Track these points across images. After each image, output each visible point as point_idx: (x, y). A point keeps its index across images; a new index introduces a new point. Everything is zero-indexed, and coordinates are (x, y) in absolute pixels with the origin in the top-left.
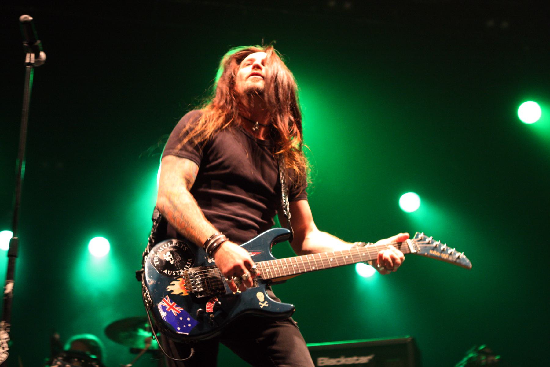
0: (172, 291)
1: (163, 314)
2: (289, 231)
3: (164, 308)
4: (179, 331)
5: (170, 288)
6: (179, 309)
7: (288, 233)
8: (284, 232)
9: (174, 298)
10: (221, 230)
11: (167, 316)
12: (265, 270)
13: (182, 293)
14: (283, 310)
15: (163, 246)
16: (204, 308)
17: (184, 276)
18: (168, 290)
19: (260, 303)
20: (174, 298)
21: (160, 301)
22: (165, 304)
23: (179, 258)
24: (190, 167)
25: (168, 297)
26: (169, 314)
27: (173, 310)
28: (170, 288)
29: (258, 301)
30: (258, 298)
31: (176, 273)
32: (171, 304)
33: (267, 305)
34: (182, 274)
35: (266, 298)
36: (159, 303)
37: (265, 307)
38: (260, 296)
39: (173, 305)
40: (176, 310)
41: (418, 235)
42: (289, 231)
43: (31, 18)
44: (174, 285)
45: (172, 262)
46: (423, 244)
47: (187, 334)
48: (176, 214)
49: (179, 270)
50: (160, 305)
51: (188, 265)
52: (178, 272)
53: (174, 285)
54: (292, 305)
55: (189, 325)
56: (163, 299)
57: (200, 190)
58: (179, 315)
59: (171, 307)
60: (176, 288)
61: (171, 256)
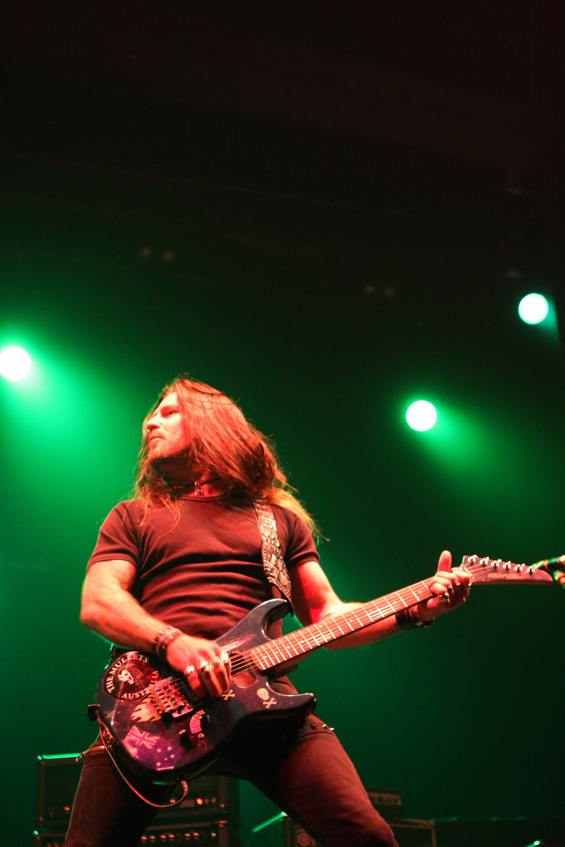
0: (139, 718)
1: (133, 751)
2: (286, 601)
3: (132, 743)
4: (160, 767)
5: (136, 715)
6: (155, 739)
7: (284, 603)
8: (278, 604)
9: (142, 726)
10: (169, 622)
11: (139, 753)
12: (261, 657)
13: (153, 718)
14: (299, 703)
15: (116, 665)
16: (188, 728)
17: (150, 694)
18: (134, 718)
19: (265, 703)
20: (142, 726)
21: (125, 734)
22: (133, 738)
23: (140, 674)
24: (122, 567)
25: (135, 728)
26: (142, 748)
27: (139, 735)
28: (136, 715)
29: (261, 700)
30: (261, 697)
31: (140, 694)
32: (141, 736)
33: (275, 703)
34: (148, 692)
35: (271, 694)
36: (124, 737)
37: (272, 705)
38: (263, 693)
39: (145, 736)
40: (150, 741)
41: (466, 560)
42: (286, 601)
43: (184, 731)
44: (140, 710)
45: (131, 682)
46: (474, 568)
47: (172, 768)
48: (111, 617)
49: (143, 689)
50: (125, 742)
51: (154, 680)
52: (142, 692)
53: (140, 710)
54: (312, 694)
55: (172, 756)
56: (128, 732)
57: (136, 588)
58: (156, 747)
59: (142, 739)
60: (143, 713)
61: (129, 675)
